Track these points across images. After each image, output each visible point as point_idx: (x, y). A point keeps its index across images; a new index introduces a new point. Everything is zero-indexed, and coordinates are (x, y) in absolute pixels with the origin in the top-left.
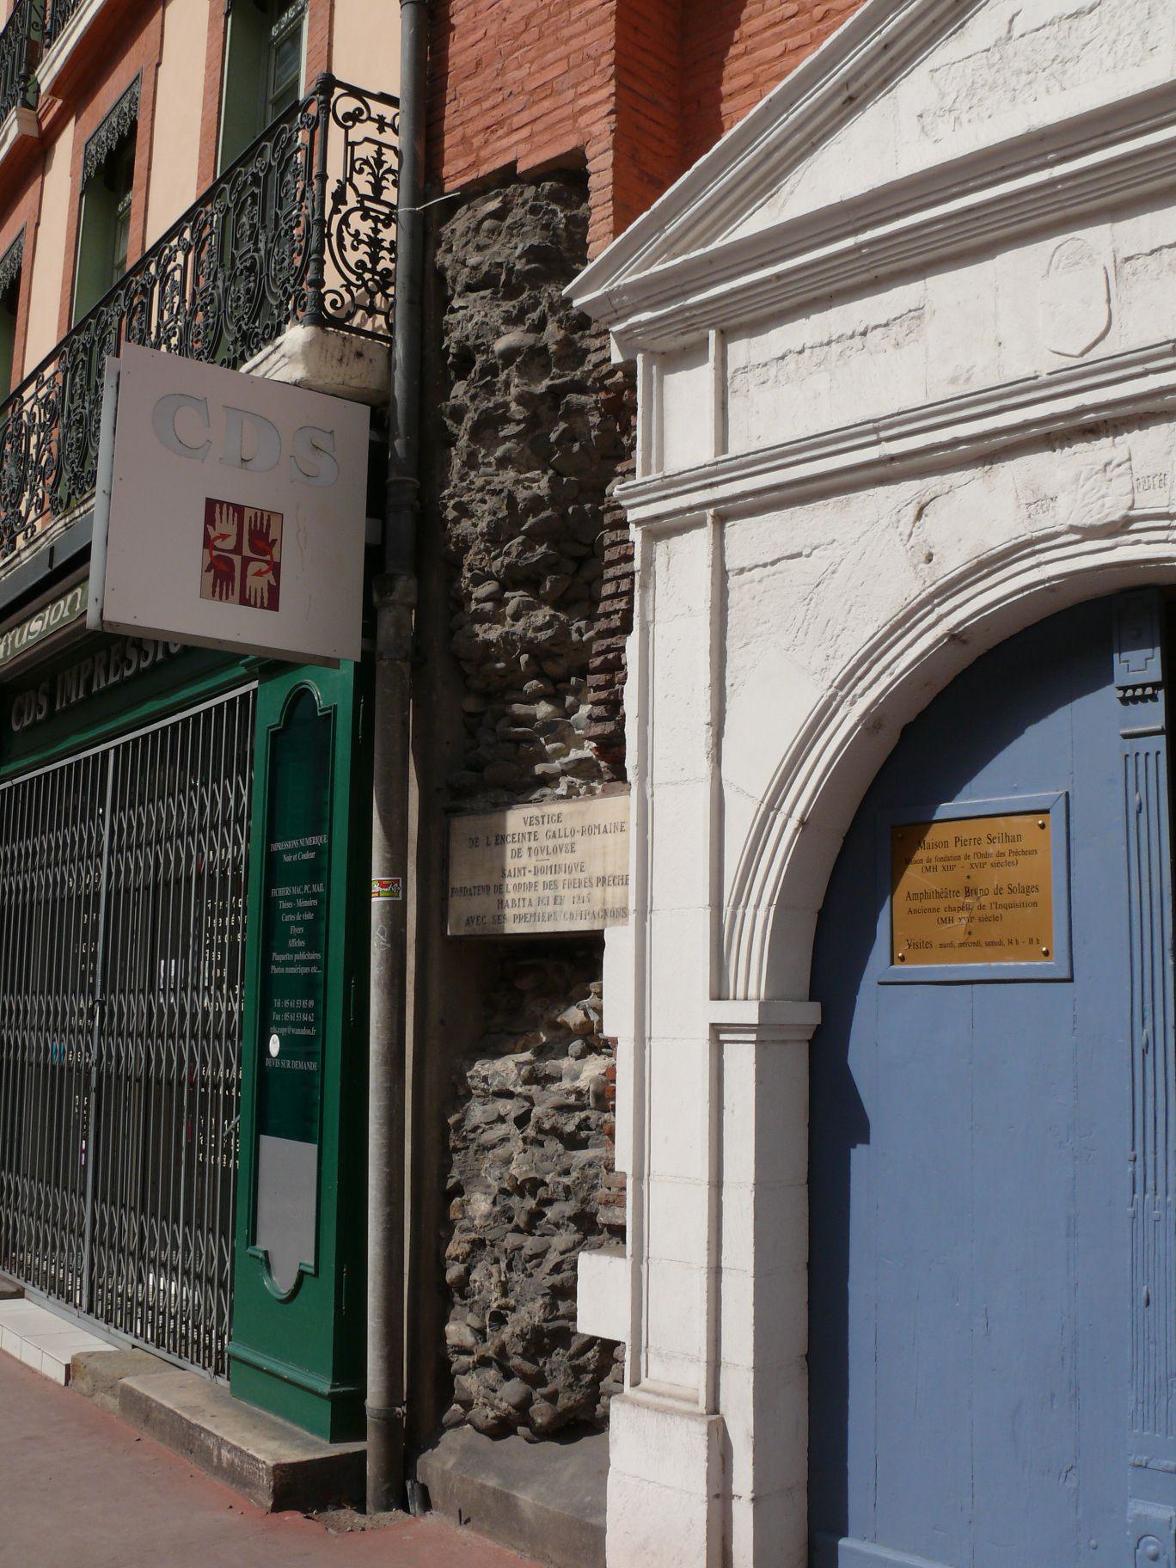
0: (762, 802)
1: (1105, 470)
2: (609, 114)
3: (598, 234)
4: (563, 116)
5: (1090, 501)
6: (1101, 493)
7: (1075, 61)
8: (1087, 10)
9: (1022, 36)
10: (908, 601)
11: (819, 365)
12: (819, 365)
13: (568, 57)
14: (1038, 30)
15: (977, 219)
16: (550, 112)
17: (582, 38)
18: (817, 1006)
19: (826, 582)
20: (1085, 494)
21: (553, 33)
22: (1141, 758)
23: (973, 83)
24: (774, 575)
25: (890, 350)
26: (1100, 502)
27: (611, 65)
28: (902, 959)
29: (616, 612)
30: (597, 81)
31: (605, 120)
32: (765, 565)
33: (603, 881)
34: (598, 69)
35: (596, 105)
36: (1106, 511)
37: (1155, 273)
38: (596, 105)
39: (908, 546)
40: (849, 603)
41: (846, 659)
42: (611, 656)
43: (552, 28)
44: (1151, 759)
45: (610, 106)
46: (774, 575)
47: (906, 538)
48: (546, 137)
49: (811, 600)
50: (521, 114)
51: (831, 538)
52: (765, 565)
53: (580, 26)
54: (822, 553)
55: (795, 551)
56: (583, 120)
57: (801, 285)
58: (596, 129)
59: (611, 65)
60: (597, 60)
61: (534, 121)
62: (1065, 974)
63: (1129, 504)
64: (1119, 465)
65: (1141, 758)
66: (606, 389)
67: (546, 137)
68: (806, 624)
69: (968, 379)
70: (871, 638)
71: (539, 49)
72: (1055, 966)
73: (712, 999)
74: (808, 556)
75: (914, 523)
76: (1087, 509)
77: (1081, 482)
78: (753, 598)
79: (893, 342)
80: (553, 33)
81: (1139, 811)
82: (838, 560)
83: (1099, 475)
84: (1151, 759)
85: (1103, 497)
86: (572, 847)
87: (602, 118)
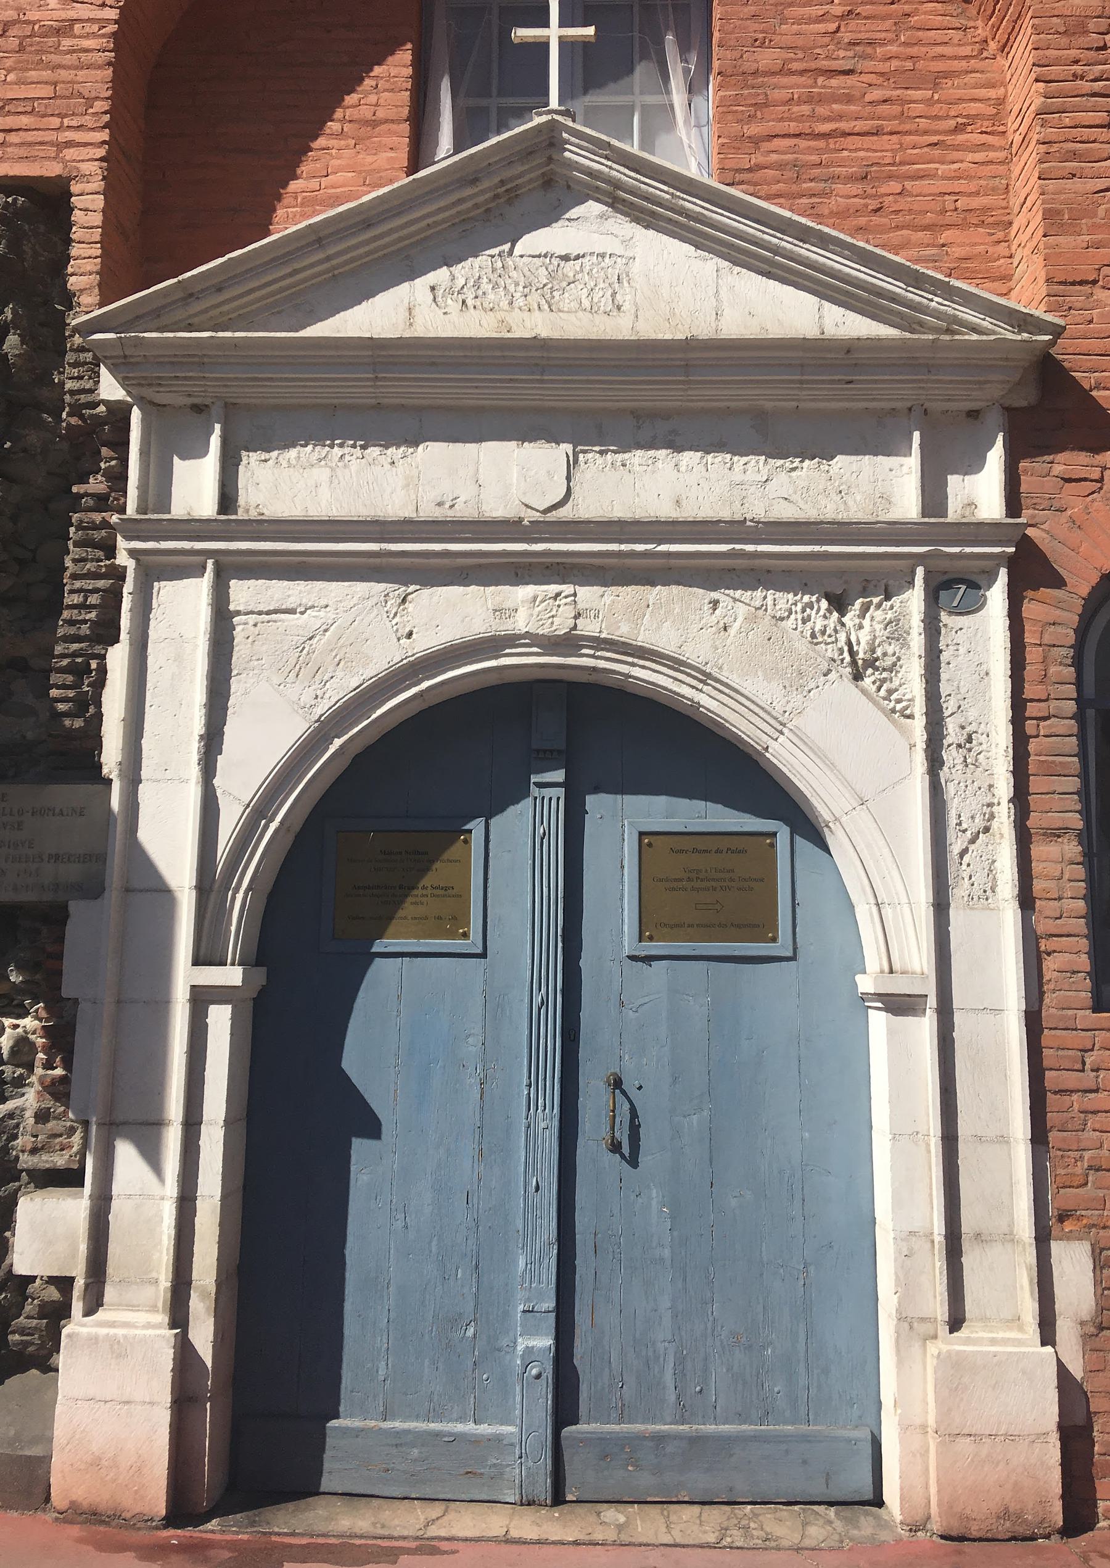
0: (248, 805)
1: (555, 600)
2: (101, 159)
3: (82, 270)
4: (47, 139)
5: (544, 617)
6: (551, 614)
7: (561, 292)
8: (572, 257)
9: (522, 256)
10: (391, 664)
11: (320, 460)
12: (320, 460)
13: (55, 84)
14: (533, 257)
15: (476, 387)
16: (29, 130)
17: (72, 72)
18: (264, 969)
19: (318, 637)
20: (540, 612)
21: (37, 52)
22: (546, 801)
23: (479, 277)
24: (268, 622)
25: (387, 466)
26: (551, 620)
27: (106, 113)
28: (651, 939)
29: (85, 622)
30: (88, 121)
31: (96, 163)
32: (260, 613)
33: (56, 858)
34: (91, 111)
35: (86, 145)
36: (554, 628)
37: (601, 467)
38: (86, 145)
39: (394, 622)
40: (338, 658)
41: (334, 700)
42: (79, 660)
43: (38, 48)
44: (554, 802)
45: (101, 152)
46: (268, 622)
47: (392, 616)
48: (23, 152)
49: (304, 648)
50: (22, 117)
51: (325, 603)
52: (260, 613)
53: (68, 59)
54: (315, 614)
55: (290, 606)
56: (70, 153)
57: (420, 391)
58: (87, 168)
59: (106, 113)
60: (90, 102)
61: (10, 131)
62: (479, 951)
63: (572, 625)
64: (566, 597)
65: (546, 801)
66: (81, 417)
67: (23, 152)
68: (298, 667)
69: (452, 506)
70: (355, 690)
71: (20, 62)
72: (473, 943)
73: (193, 965)
74: (302, 613)
75: (400, 606)
76: (541, 623)
77: (537, 603)
78: (248, 638)
79: (390, 460)
80: (37, 52)
81: (542, 839)
82: (330, 622)
83: (551, 601)
84: (554, 802)
85: (553, 616)
86: (19, 826)
87: (97, 160)
